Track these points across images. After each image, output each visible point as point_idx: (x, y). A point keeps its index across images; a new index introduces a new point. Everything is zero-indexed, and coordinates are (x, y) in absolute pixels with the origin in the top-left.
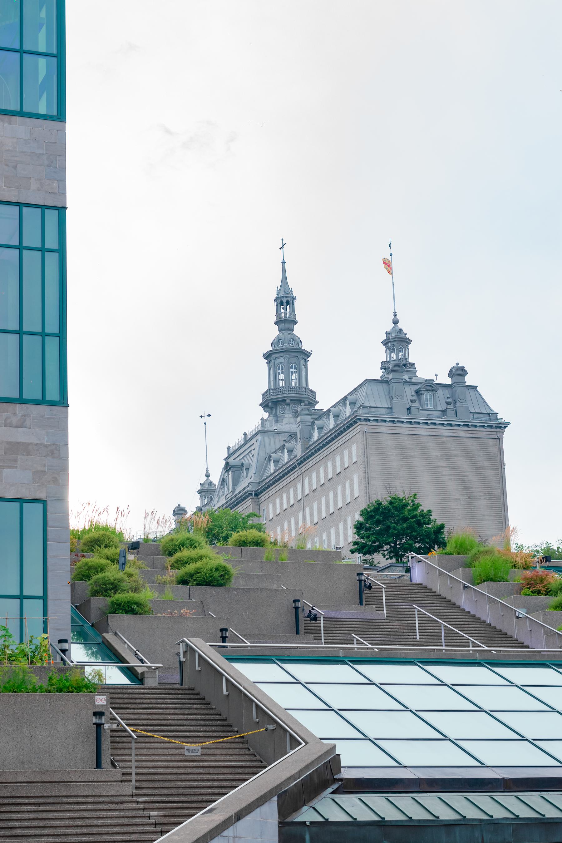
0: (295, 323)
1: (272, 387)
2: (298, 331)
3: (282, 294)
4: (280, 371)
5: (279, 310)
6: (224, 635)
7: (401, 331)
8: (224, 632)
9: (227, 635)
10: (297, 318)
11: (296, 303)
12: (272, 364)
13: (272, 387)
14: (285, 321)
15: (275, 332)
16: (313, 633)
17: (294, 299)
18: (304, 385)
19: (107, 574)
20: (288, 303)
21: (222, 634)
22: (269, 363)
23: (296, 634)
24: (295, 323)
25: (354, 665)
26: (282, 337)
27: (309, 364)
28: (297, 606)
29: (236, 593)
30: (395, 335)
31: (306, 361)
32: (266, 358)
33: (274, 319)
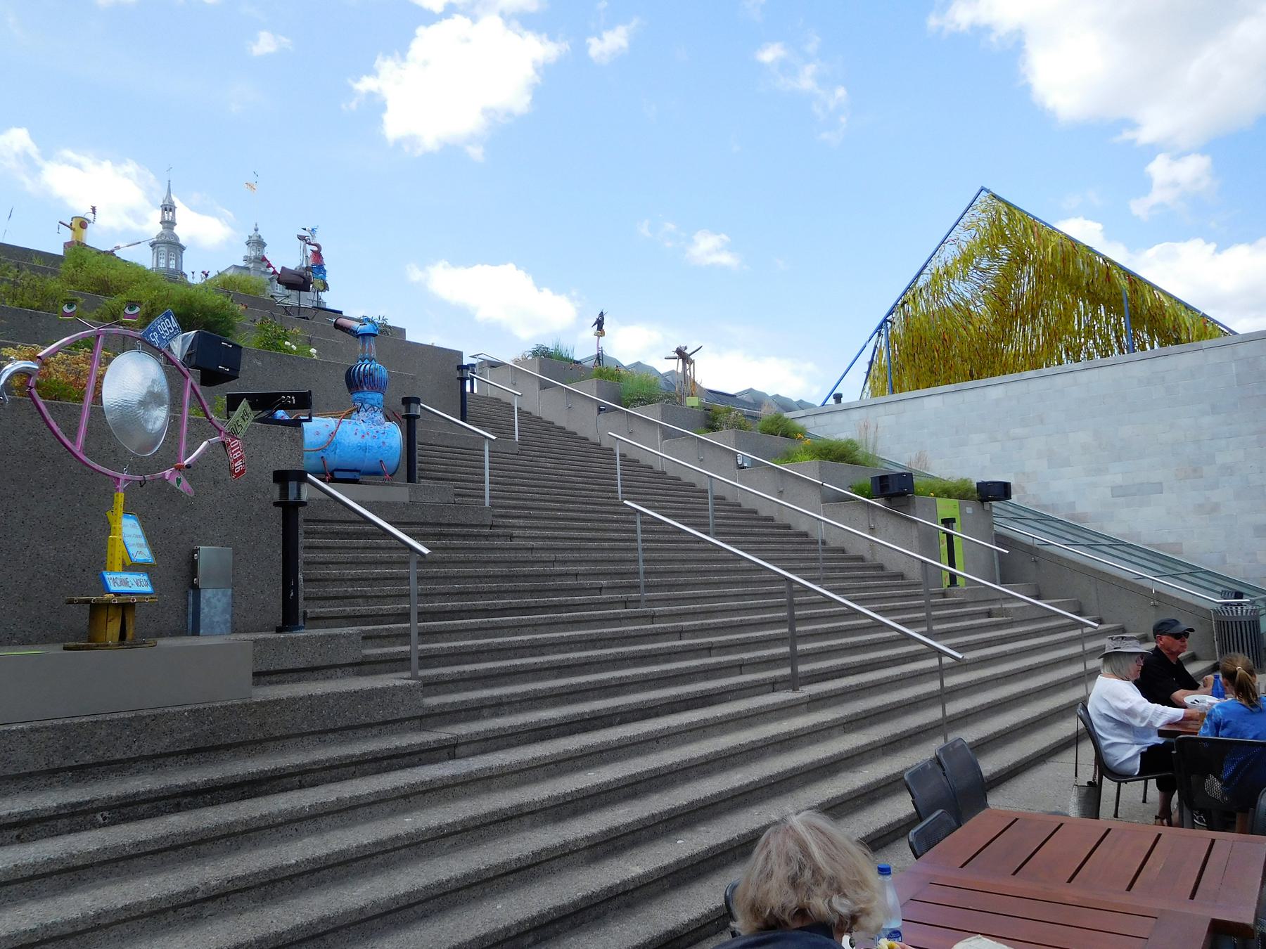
0: (175, 224)
1: (155, 266)
2: (176, 230)
3: (167, 203)
4: (162, 256)
5: (163, 214)
6: (291, 498)
7: (260, 237)
8: (292, 485)
9: (304, 497)
10: (177, 222)
11: (176, 210)
12: (155, 250)
13: (155, 266)
14: (168, 222)
15: (159, 228)
16: (452, 480)
17: (175, 207)
18: (180, 269)
19: (836, 922)
20: (171, 210)
21: (284, 491)
22: (153, 250)
23: (408, 482)
24: (175, 224)
25: (1146, 739)
26: (165, 233)
27: (184, 255)
28: (412, 413)
29: (259, 364)
30: (255, 238)
31: (182, 252)
32: (151, 246)
33: (160, 220)
